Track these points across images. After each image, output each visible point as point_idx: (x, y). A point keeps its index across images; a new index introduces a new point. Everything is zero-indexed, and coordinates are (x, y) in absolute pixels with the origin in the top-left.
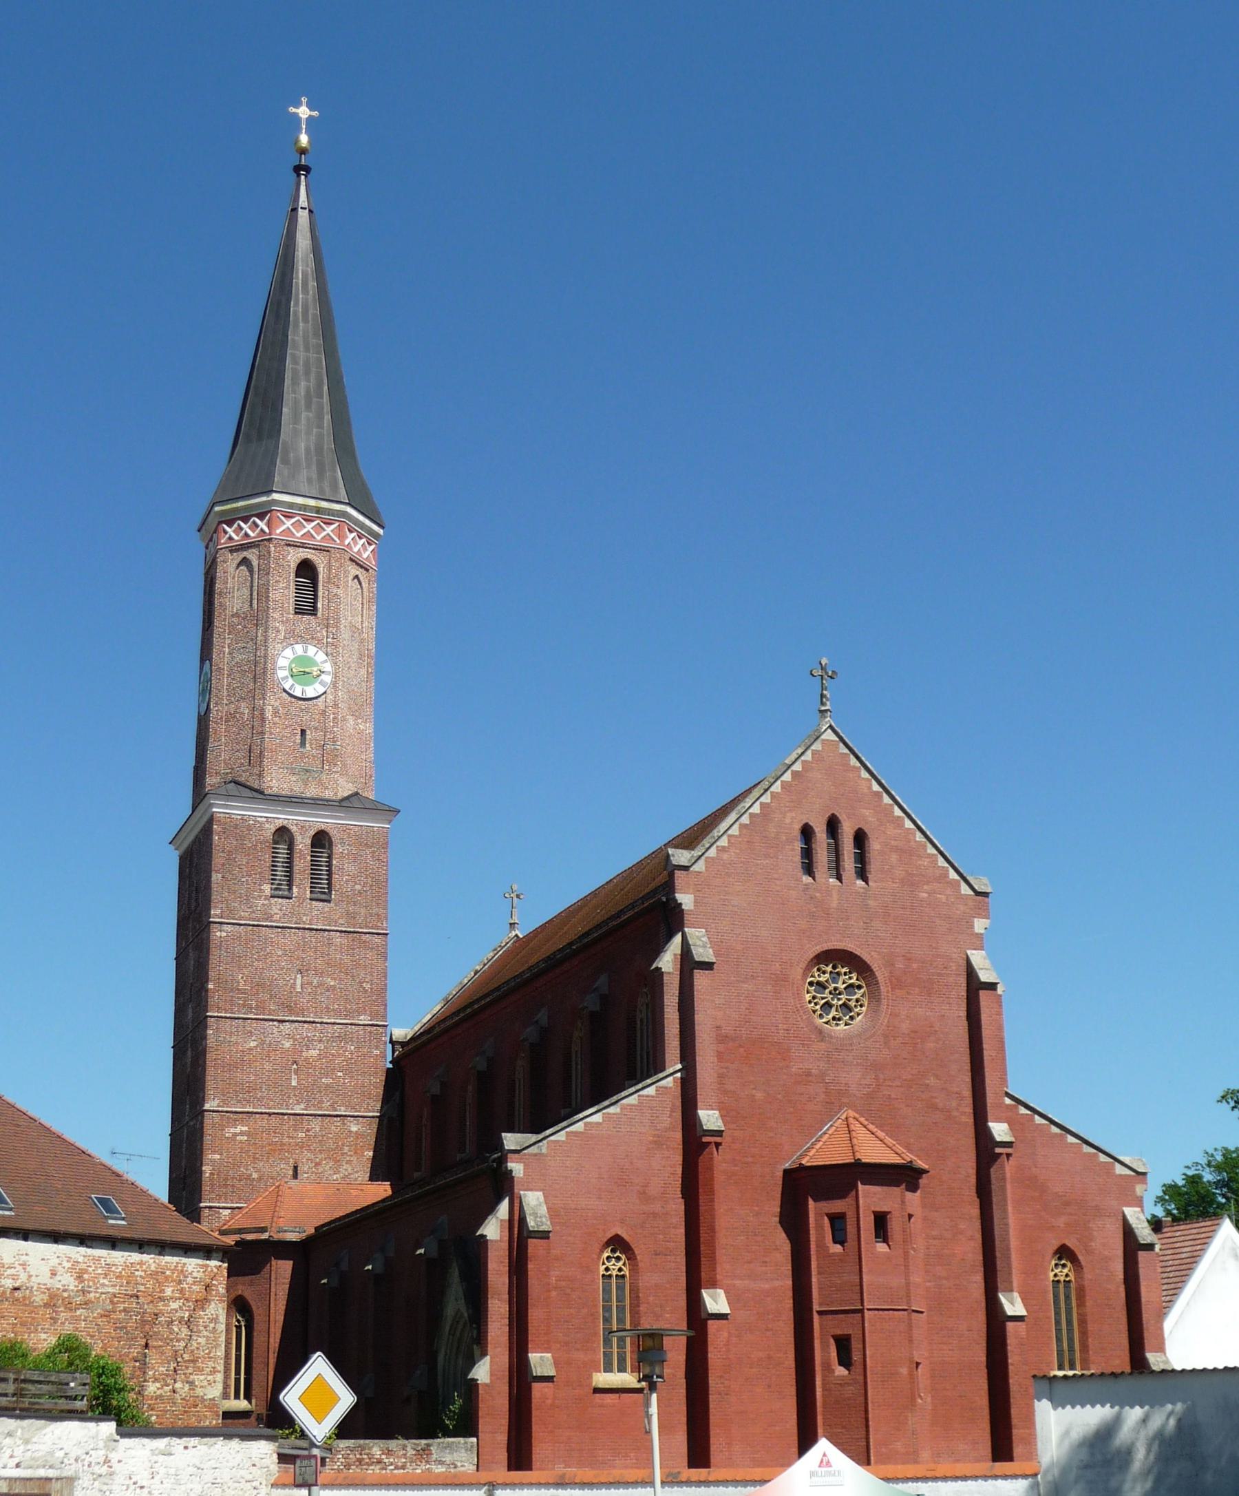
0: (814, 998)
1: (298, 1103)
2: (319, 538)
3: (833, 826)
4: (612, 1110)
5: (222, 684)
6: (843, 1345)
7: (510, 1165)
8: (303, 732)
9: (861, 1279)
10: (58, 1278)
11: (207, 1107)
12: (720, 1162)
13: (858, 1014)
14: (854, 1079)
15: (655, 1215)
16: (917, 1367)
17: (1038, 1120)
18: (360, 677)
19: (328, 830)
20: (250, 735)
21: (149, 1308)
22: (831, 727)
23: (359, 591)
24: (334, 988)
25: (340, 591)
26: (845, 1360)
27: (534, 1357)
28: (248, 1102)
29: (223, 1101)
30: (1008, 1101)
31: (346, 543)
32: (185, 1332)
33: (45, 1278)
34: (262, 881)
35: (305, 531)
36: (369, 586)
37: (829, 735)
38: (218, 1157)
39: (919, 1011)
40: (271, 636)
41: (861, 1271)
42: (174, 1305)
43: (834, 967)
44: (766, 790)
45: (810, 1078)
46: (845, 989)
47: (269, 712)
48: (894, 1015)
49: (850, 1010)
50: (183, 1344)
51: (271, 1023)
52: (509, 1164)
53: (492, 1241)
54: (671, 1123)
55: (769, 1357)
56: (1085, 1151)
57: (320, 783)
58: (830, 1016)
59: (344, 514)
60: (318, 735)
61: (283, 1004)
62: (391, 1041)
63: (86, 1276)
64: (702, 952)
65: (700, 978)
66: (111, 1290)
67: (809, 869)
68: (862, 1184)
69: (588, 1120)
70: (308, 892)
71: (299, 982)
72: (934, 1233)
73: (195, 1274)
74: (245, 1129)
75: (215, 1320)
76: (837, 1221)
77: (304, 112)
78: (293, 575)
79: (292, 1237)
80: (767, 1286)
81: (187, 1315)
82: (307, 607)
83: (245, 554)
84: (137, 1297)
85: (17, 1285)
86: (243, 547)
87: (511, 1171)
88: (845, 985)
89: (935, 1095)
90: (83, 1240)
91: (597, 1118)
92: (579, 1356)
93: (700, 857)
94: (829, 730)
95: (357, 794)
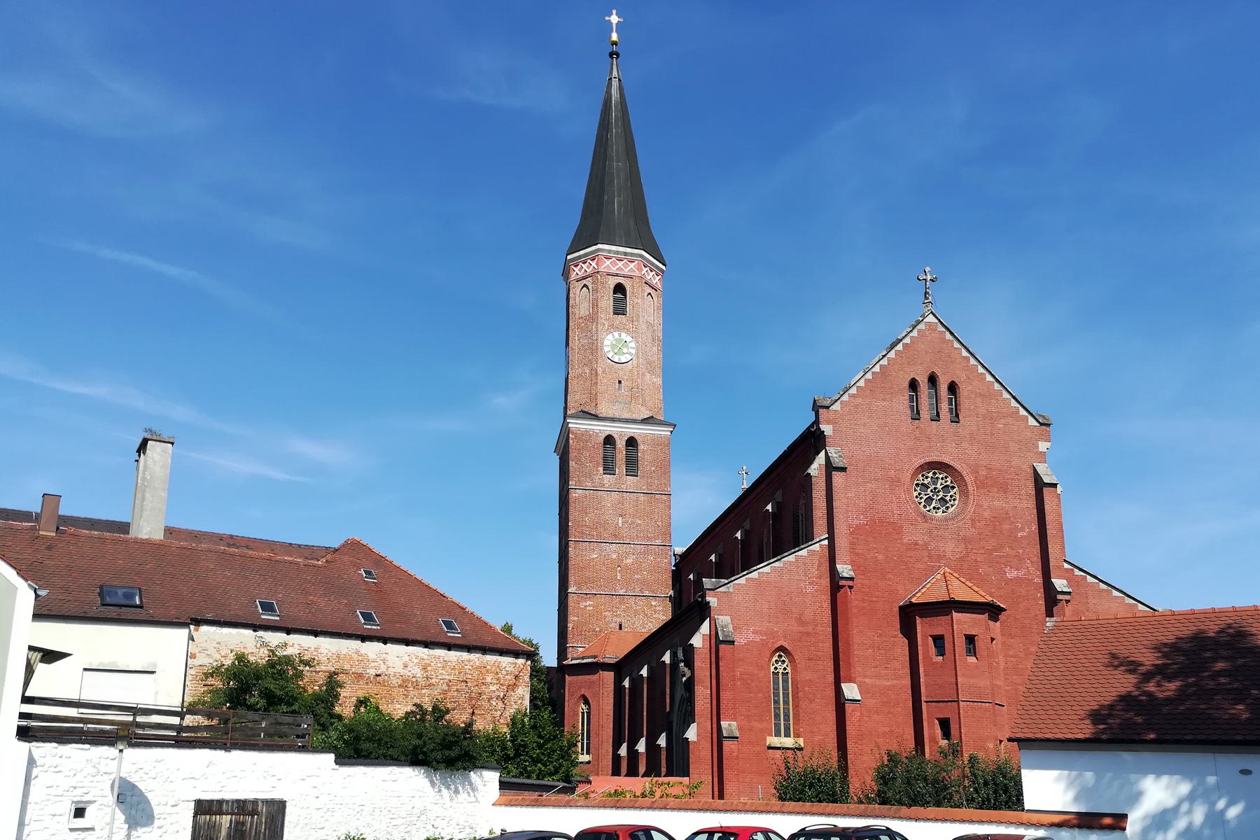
0: (920, 494)
1: (621, 589)
2: (626, 270)
3: (933, 380)
4: (777, 564)
5: (575, 357)
6: (945, 724)
7: (708, 599)
8: (620, 382)
9: (957, 679)
10: (409, 669)
11: (569, 591)
12: (853, 600)
13: (952, 506)
14: (950, 548)
15: (808, 634)
16: (1000, 743)
17: (1090, 579)
18: (654, 352)
19: (635, 437)
20: (590, 385)
21: (475, 689)
22: (932, 313)
23: (652, 303)
24: (640, 525)
25: (639, 301)
26: (947, 734)
27: (724, 724)
28: (593, 588)
29: (579, 587)
30: (1066, 566)
31: (643, 273)
32: (500, 704)
33: (399, 669)
34: (598, 464)
35: (618, 266)
36: (657, 300)
37: (931, 319)
38: (577, 618)
39: (997, 503)
40: (600, 327)
41: (956, 675)
42: (493, 688)
43: (934, 473)
44: (884, 356)
45: (917, 547)
46: (942, 488)
47: (600, 371)
48: (979, 506)
49: (947, 502)
50: (499, 713)
51: (605, 544)
52: (707, 598)
53: (697, 648)
54: (818, 574)
55: (891, 732)
56: (1127, 602)
57: (630, 410)
58: (932, 507)
59: (641, 256)
60: (629, 383)
61: (611, 533)
62: (674, 555)
63: (429, 668)
64: (837, 460)
65: (838, 478)
66: (447, 677)
67: (916, 415)
68: (955, 612)
69: (760, 570)
70: (625, 472)
71: (620, 521)
72: (1011, 653)
73: (507, 669)
74: (592, 603)
75: (522, 698)
76: (939, 640)
77: (614, 19)
78: (612, 292)
79: (612, 661)
80: (888, 684)
81: (502, 694)
82: (620, 310)
83: (584, 282)
84: (466, 682)
85: (378, 673)
86: (584, 278)
87: (709, 602)
88: (942, 486)
89: (1011, 560)
90: (427, 644)
91: (767, 569)
92: (756, 725)
93: (836, 401)
94: (931, 315)
95: (652, 417)
